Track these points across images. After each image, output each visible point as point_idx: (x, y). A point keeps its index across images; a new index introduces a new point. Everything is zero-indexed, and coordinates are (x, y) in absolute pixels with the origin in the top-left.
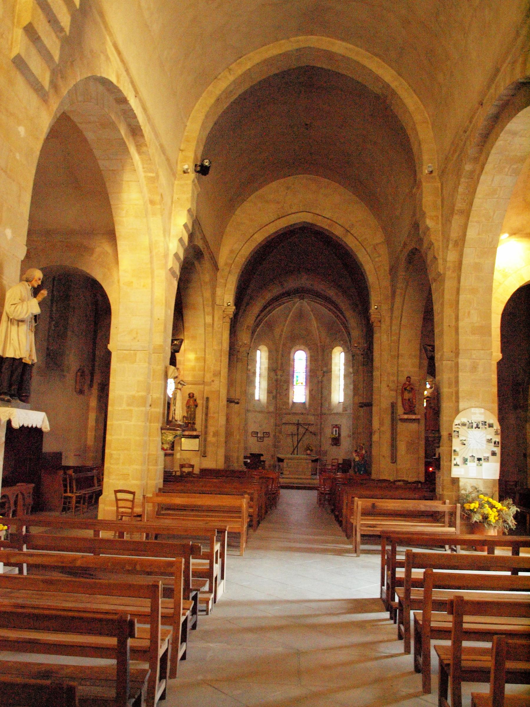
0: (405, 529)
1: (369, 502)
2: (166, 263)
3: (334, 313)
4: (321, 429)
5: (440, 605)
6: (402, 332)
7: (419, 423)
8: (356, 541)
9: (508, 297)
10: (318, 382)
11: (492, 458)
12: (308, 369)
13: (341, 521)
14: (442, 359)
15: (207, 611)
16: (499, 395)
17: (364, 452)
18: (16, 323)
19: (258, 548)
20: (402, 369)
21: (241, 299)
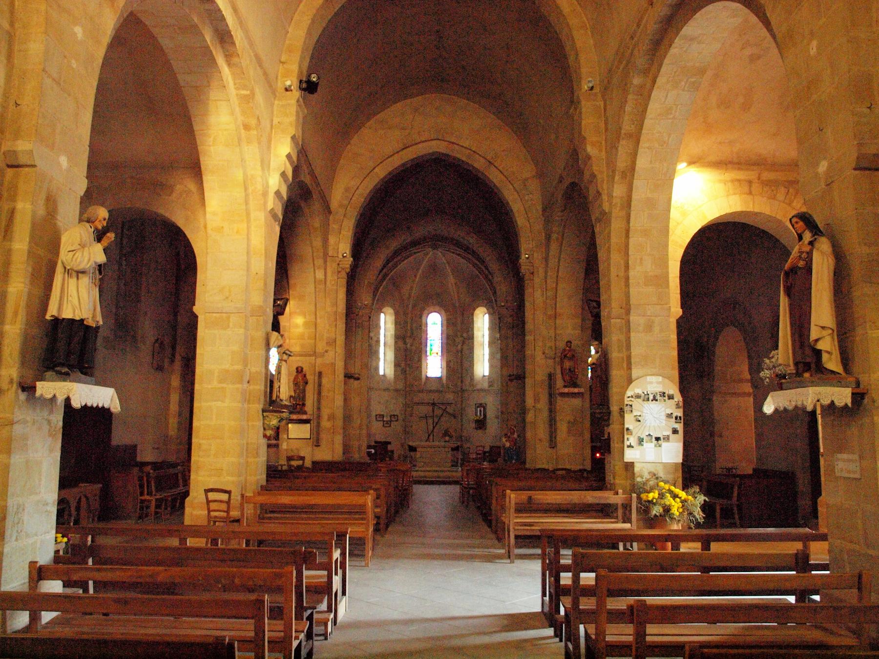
0: (569, 527)
1: (524, 496)
2: (265, 203)
3: (474, 265)
5: (617, 616)
6: (561, 286)
7: (583, 398)
8: (509, 543)
9: (688, 240)
11: (672, 437)
12: (445, 336)
13: (491, 520)
15: (325, 636)
16: (680, 361)
17: (515, 436)
18: (74, 274)
19: (390, 557)
21: (360, 248)
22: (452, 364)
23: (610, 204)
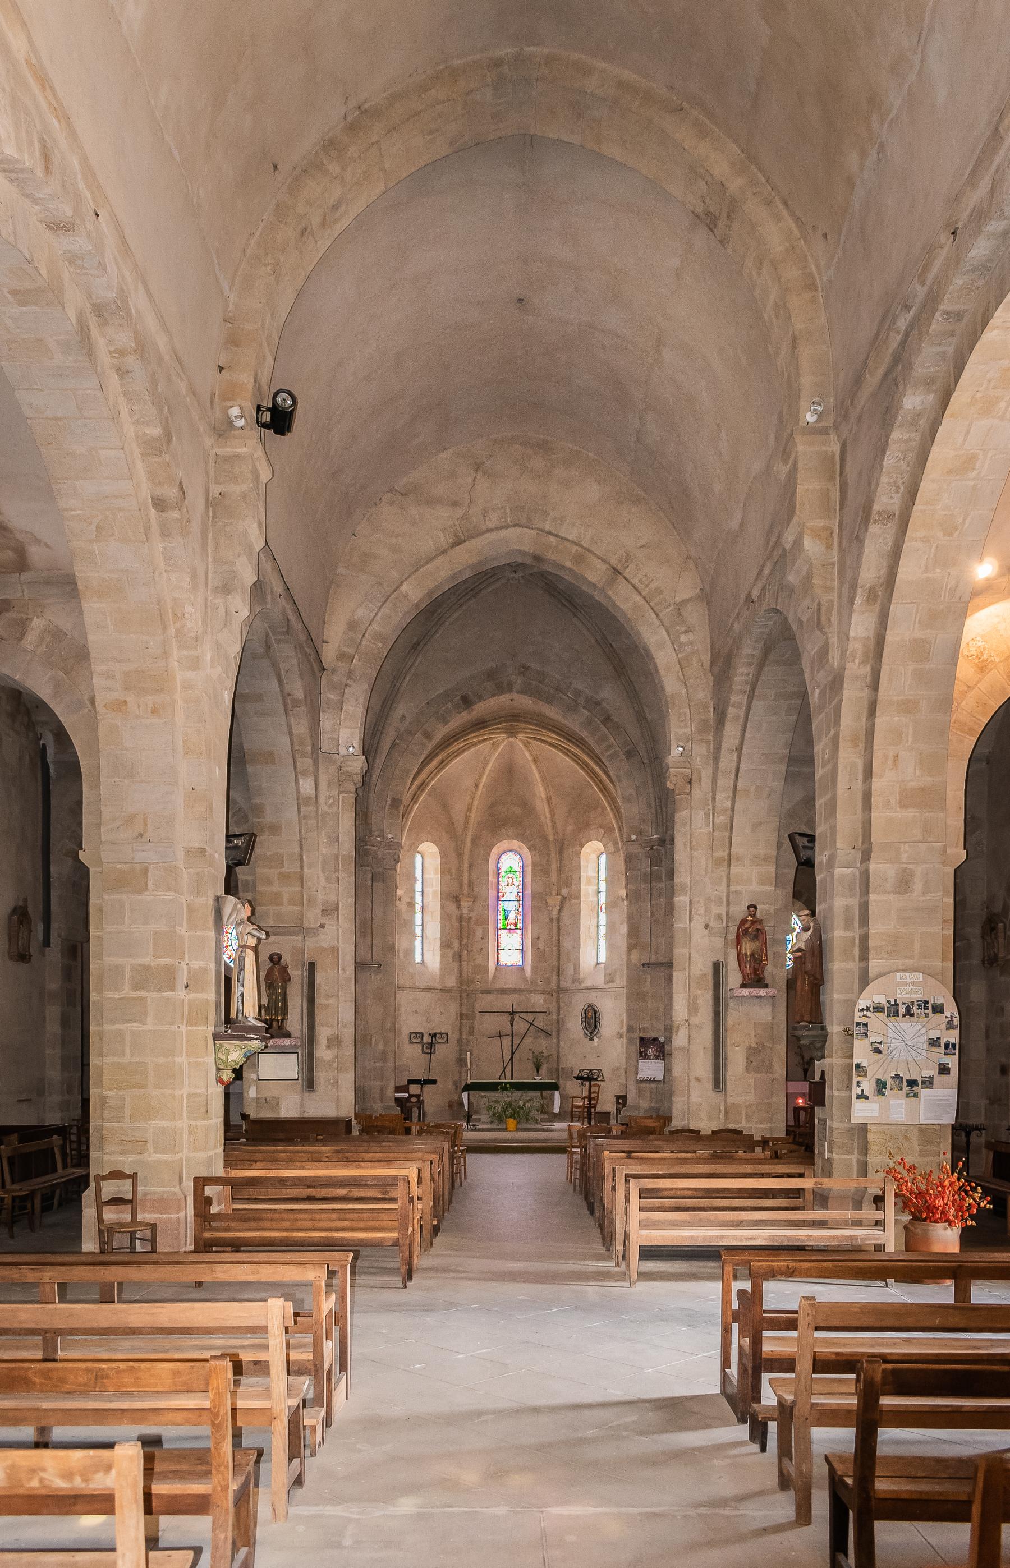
3: (584, 765)
4: (559, 1024)
10: (551, 920)
11: (938, 1079)
14: (831, 864)
20: (739, 888)
22: (541, 944)
23: (843, 654)
